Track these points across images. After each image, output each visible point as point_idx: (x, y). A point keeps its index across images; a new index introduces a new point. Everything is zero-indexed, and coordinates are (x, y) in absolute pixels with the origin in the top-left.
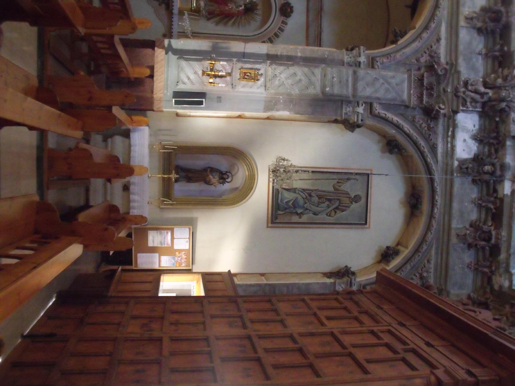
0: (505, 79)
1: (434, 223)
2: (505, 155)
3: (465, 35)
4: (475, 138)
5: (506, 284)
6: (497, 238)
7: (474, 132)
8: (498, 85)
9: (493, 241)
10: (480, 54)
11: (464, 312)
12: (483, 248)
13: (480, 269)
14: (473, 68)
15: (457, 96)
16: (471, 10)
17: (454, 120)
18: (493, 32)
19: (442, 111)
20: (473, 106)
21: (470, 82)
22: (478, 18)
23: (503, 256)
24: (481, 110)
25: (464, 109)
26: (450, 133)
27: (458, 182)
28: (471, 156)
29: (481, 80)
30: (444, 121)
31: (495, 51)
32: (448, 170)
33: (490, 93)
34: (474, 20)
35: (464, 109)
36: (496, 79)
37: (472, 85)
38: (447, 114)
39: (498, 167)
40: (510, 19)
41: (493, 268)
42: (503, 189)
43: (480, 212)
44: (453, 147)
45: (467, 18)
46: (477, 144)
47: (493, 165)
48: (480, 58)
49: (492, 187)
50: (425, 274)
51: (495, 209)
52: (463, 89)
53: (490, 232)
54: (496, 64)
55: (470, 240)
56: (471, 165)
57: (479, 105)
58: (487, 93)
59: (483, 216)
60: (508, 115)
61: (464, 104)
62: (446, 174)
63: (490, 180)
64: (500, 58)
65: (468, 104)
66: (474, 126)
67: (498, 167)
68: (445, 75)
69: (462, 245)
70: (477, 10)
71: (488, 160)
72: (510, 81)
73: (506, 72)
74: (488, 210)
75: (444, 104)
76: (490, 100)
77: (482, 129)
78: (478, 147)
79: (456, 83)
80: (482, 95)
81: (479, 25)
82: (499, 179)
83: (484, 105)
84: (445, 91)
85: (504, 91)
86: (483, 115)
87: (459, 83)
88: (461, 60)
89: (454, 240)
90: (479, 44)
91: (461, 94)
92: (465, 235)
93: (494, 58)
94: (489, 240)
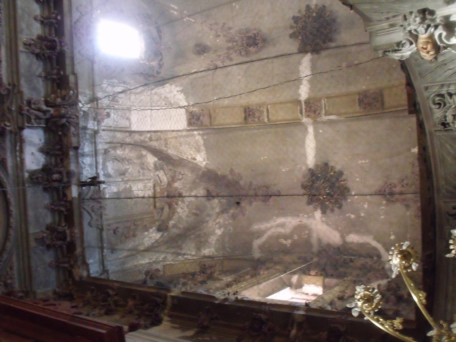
0: (63, 98)
1: (12, 232)
2: (69, 163)
3: (25, 59)
4: (41, 150)
5: (85, 274)
6: (72, 237)
7: (41, 145)
8: (57, 103)
9: (68, 239)
10: (40, 76)
11: (44, 308)
12: (61, 247)
13: (61, 265)
14: (34, 89)
15: (22, 115)
16: (28, 37)
17: (21, 137)
18: (50, 58)
19: (8, 128)
20: (38, 123)
21: (32, 101)
22: (35, 45)
23: (78, 250)
24: (44, 126)
25: (30, 125)
26: (18, 148)
27: (30, 192)
28: (40, 167)
29: (43, 99)
30: (11, 137)
31: (53, 75)
32: (19, 182)
33: (52, 110)
34: (32, 46)
35: (30, 125)
36: (55, 99)
37: (35, 104)
38: (13, 131)
39: (65, 175)
40: (63, 48)
41: (72, 263)
42: (71, 193)
43: (54, 217)
44: (22, 161)
45: (25, 44)
46: (44, 156)
47: (60, 173)
48: (40, 80)
49: (61, 193)
50: (9, 281)
51: (67, 211)
52: (27, 108)
53: (64, 232)
54: (55, 85)
55: (48, 242)
56: (40, 175)
57: (42, 121)
58: (49, 111)
59: (57, 218)
60: (69, 130)
61: (29, 121)
62: (18, 185)
63: (59, 186)
64: (58, 81)
65: (33, 120)
66: (40, 140)
67: (65, 175)
68: (8, 95)
69: (41, 247)
70: (34, 37)
71: (56, 169)
72: (68, 100)
73: (64, 92)
74: (60, 212)
75: (9, 121)
76: (52, 116)
77: (47, 142)
78: (45, 159)
79: (19, 102)
80: (45, 112)
81: (37, 51)
82: (67, 185)
83: (47, 121)
84: (10, 110)
85: (64, 109)
86: (47, 130)
87: (23, 103)
88: (22, 82)
89: (33, 244)
90: (38, 68)
91: (25, 112)
92: (43, 238)
93: (53, 80)
94: (64, 239)
